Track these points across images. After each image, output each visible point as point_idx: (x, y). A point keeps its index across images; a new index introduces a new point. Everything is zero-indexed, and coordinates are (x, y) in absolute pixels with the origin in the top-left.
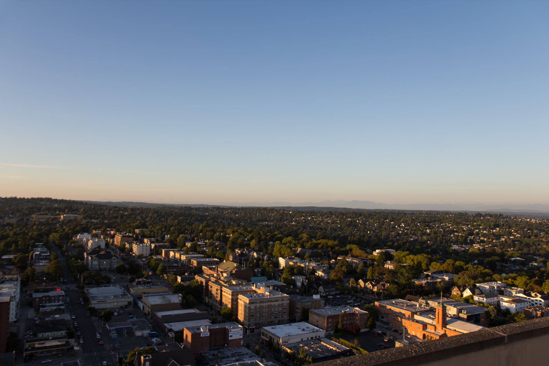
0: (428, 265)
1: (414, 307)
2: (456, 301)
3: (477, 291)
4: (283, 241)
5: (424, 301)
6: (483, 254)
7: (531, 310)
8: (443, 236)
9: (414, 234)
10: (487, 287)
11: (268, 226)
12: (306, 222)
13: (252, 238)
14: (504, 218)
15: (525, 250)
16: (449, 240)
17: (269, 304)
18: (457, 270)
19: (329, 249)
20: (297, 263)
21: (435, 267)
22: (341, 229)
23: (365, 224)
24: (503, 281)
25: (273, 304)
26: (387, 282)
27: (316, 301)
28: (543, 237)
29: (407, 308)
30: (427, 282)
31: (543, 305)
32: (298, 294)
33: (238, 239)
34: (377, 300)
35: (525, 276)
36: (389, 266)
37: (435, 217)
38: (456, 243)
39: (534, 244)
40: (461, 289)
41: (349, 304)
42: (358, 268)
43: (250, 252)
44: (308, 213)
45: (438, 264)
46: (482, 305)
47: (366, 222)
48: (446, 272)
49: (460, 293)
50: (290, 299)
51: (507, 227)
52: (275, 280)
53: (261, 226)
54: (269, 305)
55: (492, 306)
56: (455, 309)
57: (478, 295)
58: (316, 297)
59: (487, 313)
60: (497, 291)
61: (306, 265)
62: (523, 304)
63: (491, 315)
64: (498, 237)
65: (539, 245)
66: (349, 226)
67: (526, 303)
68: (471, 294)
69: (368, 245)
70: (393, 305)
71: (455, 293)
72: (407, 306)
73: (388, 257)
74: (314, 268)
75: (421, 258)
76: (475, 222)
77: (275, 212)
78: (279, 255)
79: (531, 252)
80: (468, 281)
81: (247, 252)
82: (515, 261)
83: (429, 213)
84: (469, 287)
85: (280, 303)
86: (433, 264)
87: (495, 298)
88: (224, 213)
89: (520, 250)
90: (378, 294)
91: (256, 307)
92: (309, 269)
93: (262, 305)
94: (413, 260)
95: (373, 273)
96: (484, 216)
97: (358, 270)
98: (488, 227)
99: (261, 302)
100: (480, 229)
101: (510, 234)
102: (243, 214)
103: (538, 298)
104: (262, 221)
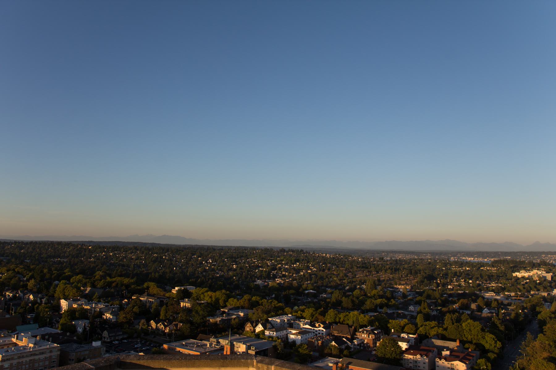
0: (225, 301)
1: (204, 347)
2: (248, 337)
3: (269, 326)
4: (72, 279)
5: (215, 340)
6: (281, 287)
8: (248, 271)
9: (220, 270)
10: (278, 321)
11: (60, 263)
12: (107, 258)
13: (31, 278)
14: (304, 253)
15: (320, 283)
16: (254, 275)
17: (32, 358)
18: (253, 305)
19: (124, 288)
20: (82, 304)
21: (232, 303)
22: (145, 265)
23: (171, 260)
24: (294, 314)
25: (37, 357)
26: (181, 322)
27: (96, 348)
29: (197, 349)
30: (222, 319)
32: (75, 342)
33: (11, 279)
34: (166, 342)
35: (313, 307)
36: (185, 304)
37: (243, 253)
38: (260, 278)
39: (327, 277)
40: (254, 324)
42: (152, 308)
43: (24, 294)
44: (110, 247)
45: (235, 300)
46: (271, 339)
47: (173, 257)
48: (242, 308)
49: (252, 328)
50: (61, 351)
51: (306, 262)
52: (52, 327)
53: (51, 263)
54: (31, 360)
55: (280, 340)
56: (244, 346)
57: (270, 329)
58: (96, 344)
59: (275, 347)
60: (288, 324)
61: (92, 307)
62: (307, 335)
63: (278, 349)
64: (298, 271)
65: (331, 277)
66: (154, 262)
67: (310, 334)
68: (263, 329)
69: (165, 282)
70: (183, 346)
71: (248, 329)
72: (198, 346)
73: (185, 294)
74: (102, 310)
75: (219, 294)
76: (279, 257)
77: (71, 248)
78: (62, 297)
79: (325, 284)
80: (261, 316)
81: (22, 295)
82: (308, 293)
83: (237, 249)
84: (261, 322)
85: (48, 355)
86: (231, 300)
87: (285, 331)
88: (6, 247)
89: (315, 283)
90: (170, 335)
91: (11, 364)
92: (95, 311)
93: (20, 360)
94: (211, 297)
95: (167, 312)
96: (287, 252)
97: (152, 310)
98: (290, 262)
99: (19, 358)
100: (282, 264)
101: (308, 268)
102: (30, 250)
103: (321, 328)
104: (54, 257)
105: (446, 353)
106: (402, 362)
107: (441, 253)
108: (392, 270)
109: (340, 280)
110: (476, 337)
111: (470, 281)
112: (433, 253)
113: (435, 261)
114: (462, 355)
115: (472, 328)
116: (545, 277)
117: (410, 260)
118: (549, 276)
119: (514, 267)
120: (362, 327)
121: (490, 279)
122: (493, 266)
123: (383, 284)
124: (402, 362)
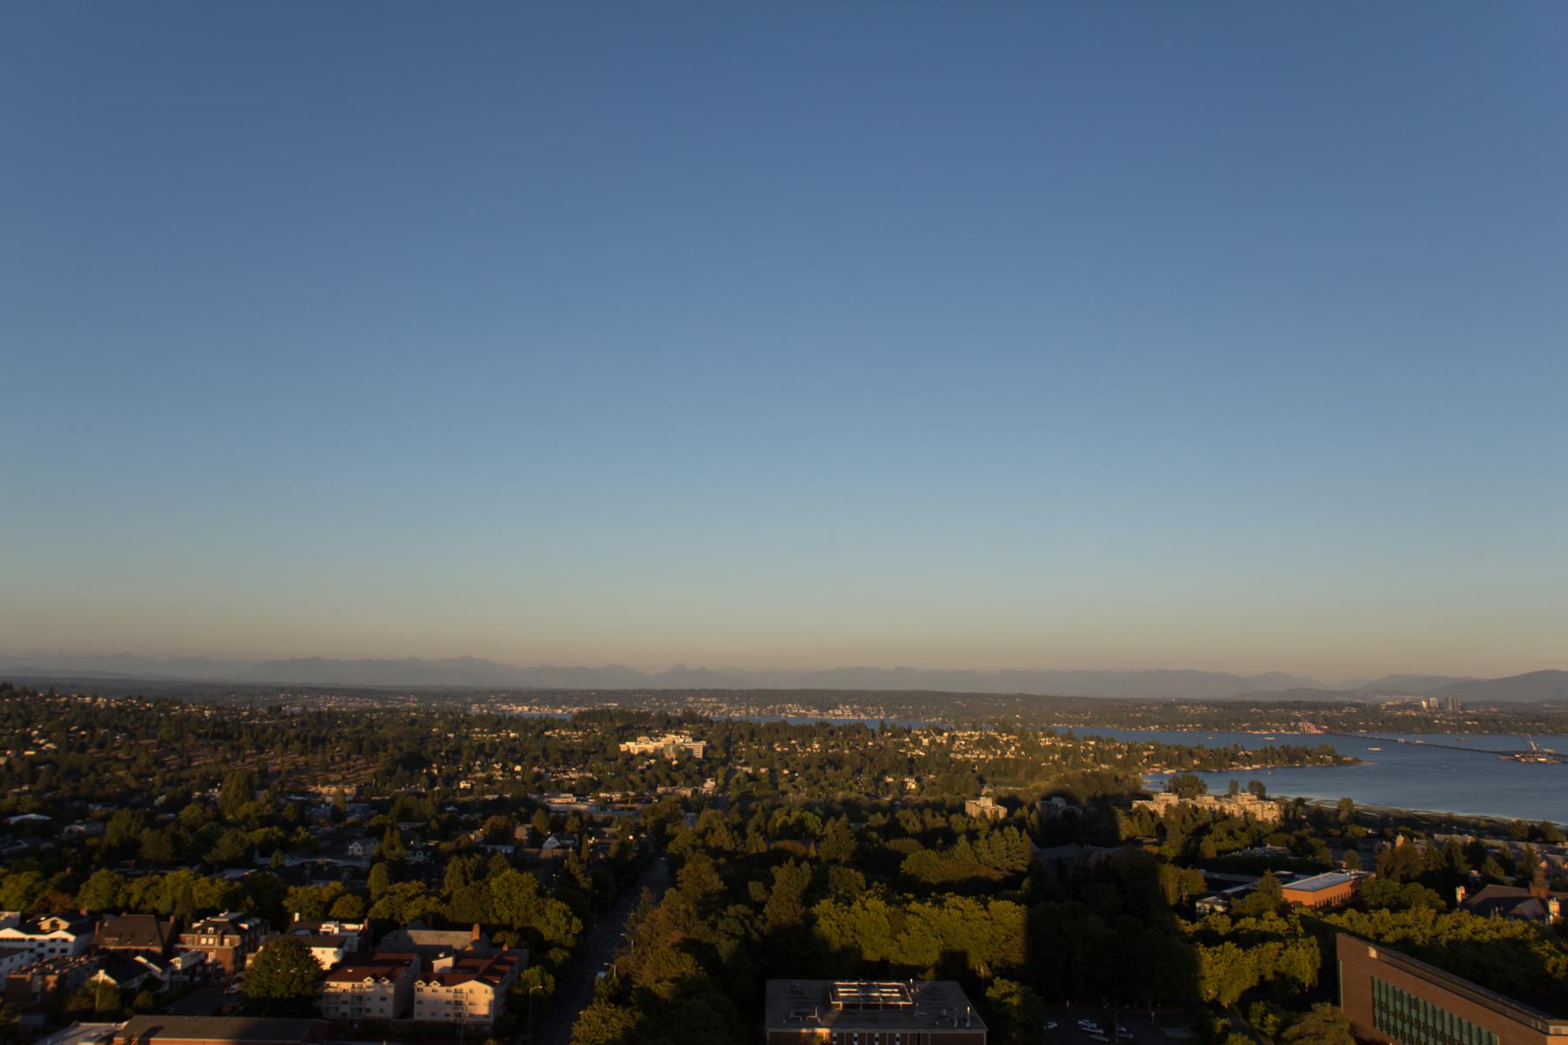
7: (28, 976)
14: (16, 695)
28: (119, 748)
31: (70, 952)
39: (92, 768)
41: (652, 757)
65: (106, 769)
67: (17, 957)
89: (49, 788)
101: (27, 741)
103: (60, 934)
105: (443, 963)
107: (445, 694)
109: (138, 777)
111: (518, 768)
112: (424, 695)
113: (429, 715)
114: (484, 964)
115: (515, 890)
116: (690, 751)
118: (698, 749)
121: (566, 762)
122: (576, 728)
123: (275, 782)
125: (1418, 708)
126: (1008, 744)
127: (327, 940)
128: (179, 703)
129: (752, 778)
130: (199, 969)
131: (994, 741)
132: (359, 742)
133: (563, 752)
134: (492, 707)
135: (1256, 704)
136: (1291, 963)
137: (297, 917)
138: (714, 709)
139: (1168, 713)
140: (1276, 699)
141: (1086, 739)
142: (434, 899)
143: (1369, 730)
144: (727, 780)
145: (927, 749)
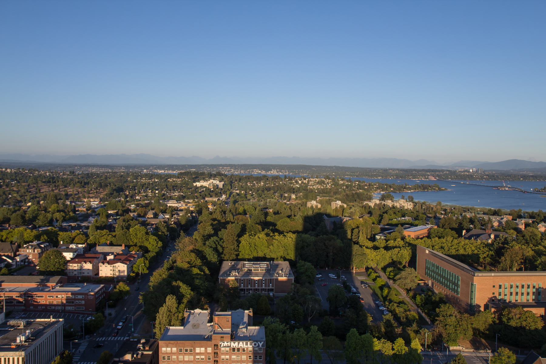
40: (123, 257)
65: (10, 194)
105: (110, 257)
106: (66, 271)
107: (134, 167)
108: (81, 183)
109: (21, 196)
110: (140, 240)
111: (157, 192)
112: (127, 167)
113: (128, 174)
114: (123, 257)
115: (138, 232)
116: (217, 185)
117: (104, 173)
118: (221, 185)
119: (196, 177)
120: (26, 243)
121: (174, 190)
122: (178, 178)
123: (71, 198)
124: (66, 271)
125: (469, 172)
126: (328, 183)
127: (71, 250)
128: (37, 171)
129: (238, 194)
130: (27, 260)
131: (324, 182)
132: (100, 183)
133: (173, 187)
134: (151, 170)
135: (415, 170)
136: (402, 255)
137: (62, 242)
138: (229, 171)
139: (385, 172)
140: (422, 169)
141: (355, 181)
142: (110, 236)
143: (451, 178)
144: (230, 196)
145: (300, 185)
